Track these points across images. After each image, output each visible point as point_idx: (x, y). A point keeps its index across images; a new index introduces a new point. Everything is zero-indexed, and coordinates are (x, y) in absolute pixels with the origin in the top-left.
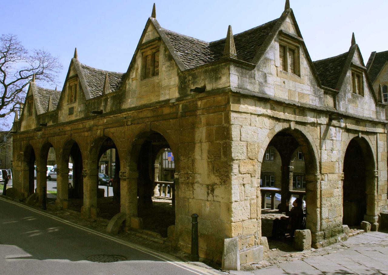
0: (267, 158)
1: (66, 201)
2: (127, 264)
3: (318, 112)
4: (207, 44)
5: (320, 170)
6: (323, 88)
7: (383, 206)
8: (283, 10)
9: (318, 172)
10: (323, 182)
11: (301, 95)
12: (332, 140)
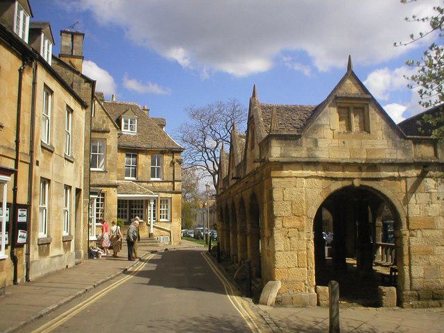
3: (404, 166)
5: (408, 225)
6: (408, 139)
9: (405, 226)
10: (412, 239)
12: (430, 193)
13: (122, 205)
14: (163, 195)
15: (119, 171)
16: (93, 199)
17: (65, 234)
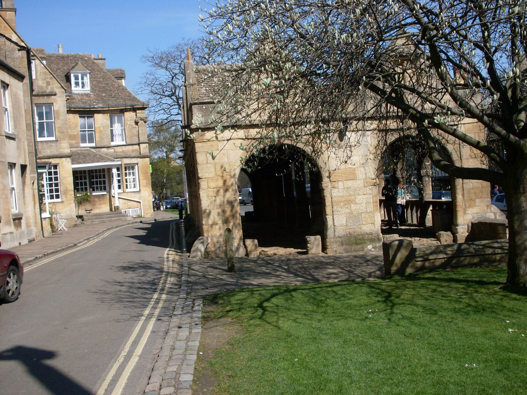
13: (100, 176)
14: (127, 161)
15: (72, 137)
16: (42, 173)
17: (15, 211)
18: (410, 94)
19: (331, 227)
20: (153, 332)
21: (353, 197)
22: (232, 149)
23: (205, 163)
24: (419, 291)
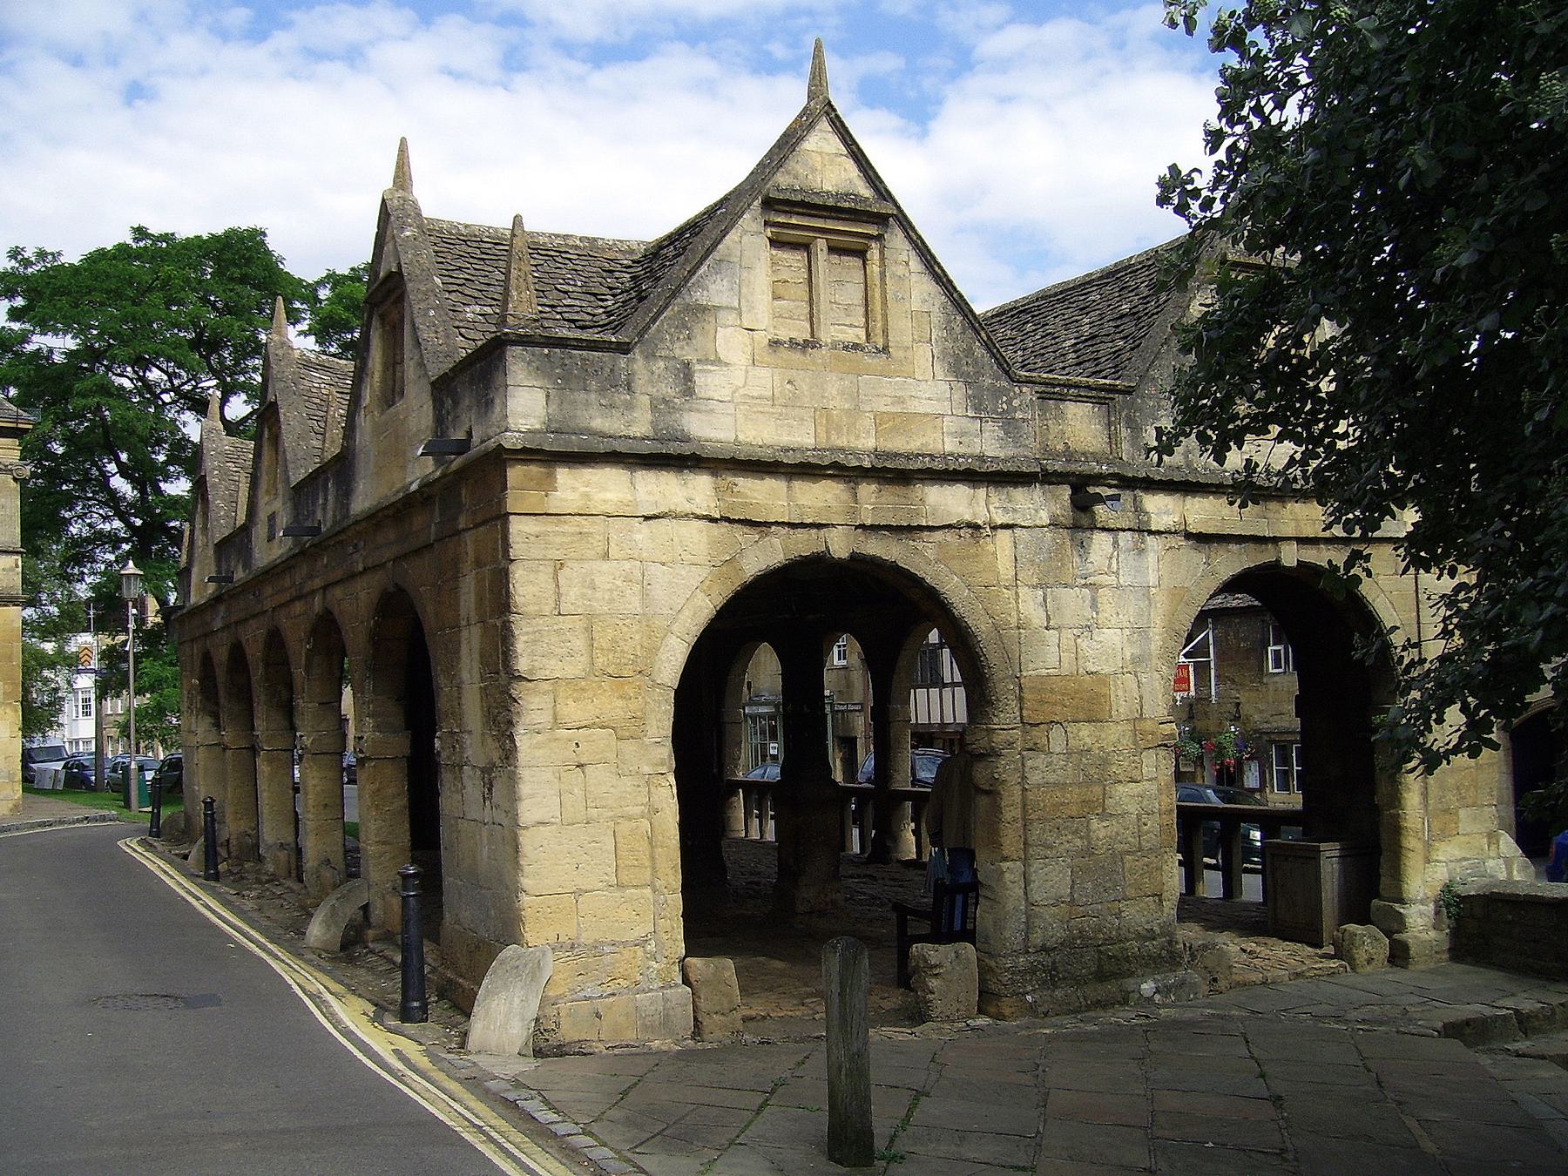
0: (1277, 666)
1: (527, 1000)
2: (1215, 1009)
4: (632, 252)
7: (1466, 859)
8: (801, 101)
11: (904, 421)
18: (519, 596)
19: (1016, 909)
20: (210, 873)
21: (1098, 790)
22: (663, 559)
23: (547, 610)
24: (1275, 173)
